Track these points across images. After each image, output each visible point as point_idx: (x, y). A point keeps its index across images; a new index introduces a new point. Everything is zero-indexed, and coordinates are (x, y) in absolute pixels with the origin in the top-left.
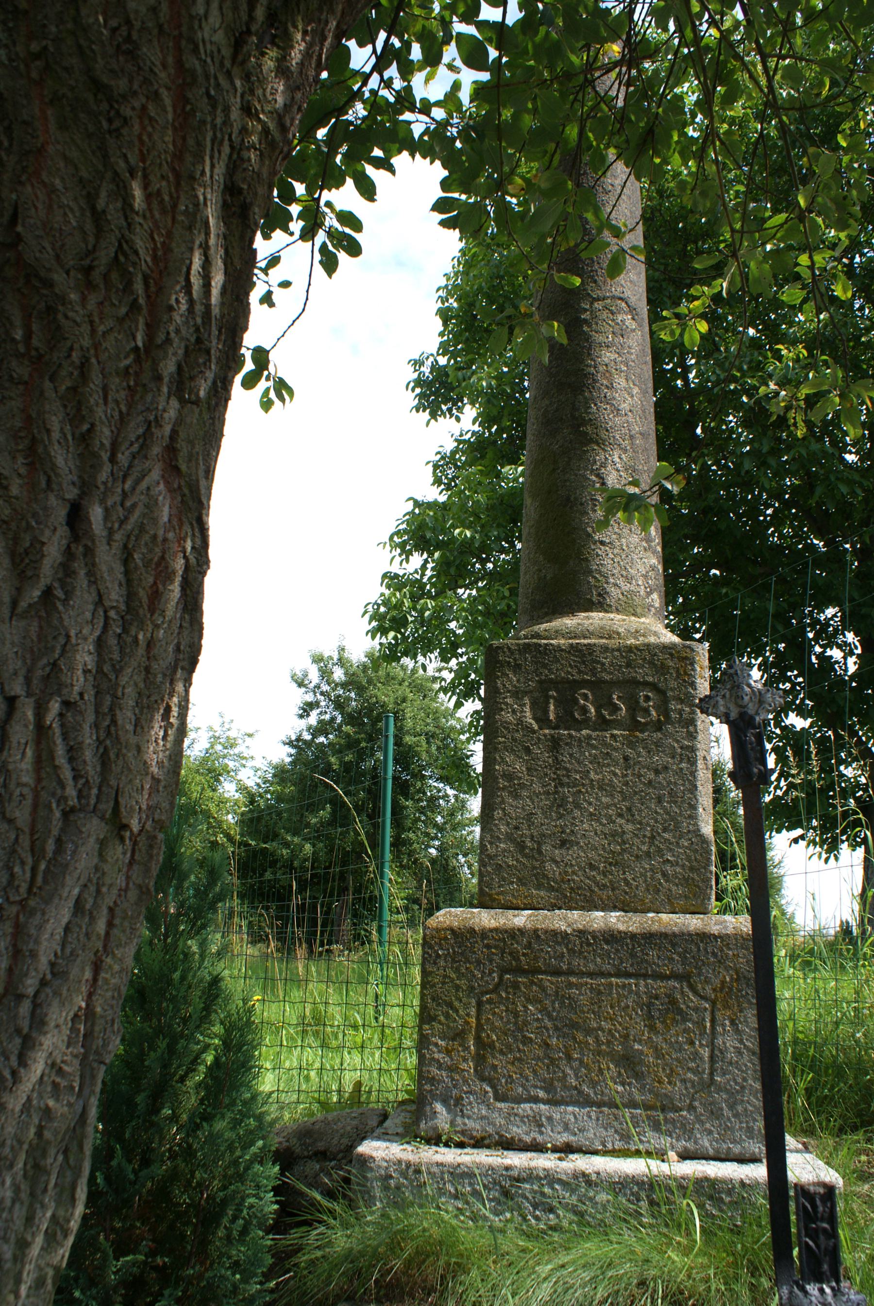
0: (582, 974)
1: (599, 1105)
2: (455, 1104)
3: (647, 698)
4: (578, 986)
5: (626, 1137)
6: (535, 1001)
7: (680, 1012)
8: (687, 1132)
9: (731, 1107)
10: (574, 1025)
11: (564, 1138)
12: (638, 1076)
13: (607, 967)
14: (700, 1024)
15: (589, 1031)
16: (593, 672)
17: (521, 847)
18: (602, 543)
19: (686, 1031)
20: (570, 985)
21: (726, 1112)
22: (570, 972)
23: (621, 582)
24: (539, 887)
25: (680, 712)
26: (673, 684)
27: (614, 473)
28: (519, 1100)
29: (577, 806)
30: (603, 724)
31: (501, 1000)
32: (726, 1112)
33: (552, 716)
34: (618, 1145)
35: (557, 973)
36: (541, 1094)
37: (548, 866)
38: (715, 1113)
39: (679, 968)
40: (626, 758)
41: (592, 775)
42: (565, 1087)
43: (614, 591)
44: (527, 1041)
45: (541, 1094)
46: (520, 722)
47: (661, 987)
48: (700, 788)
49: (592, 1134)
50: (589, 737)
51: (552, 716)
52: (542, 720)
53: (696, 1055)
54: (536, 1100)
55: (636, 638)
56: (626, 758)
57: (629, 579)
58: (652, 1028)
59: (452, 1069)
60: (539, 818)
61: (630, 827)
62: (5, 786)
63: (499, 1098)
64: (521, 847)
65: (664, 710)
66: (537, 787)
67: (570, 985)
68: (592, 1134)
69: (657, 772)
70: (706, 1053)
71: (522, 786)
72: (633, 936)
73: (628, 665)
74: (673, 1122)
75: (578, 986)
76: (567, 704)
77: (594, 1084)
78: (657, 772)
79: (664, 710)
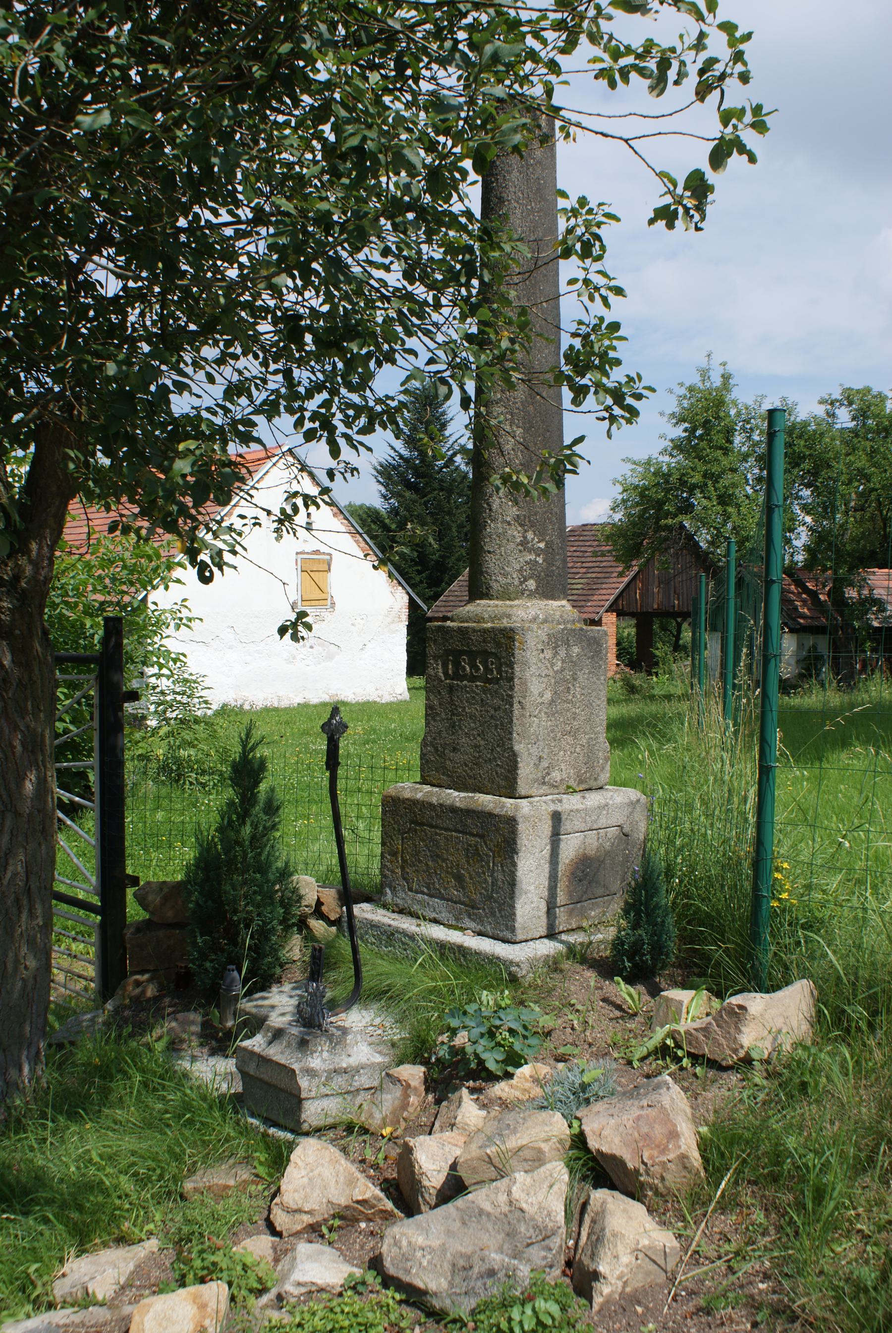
0: (441, 829)
1: (448, 900)
2: (394, 890)
3: (492, 663)
4: (440, 835)
5: (457, 919)
6: (423, 840)
7: (479, 855)
8: (482, 922)
9: (500, 912)
10: (438, 856)
11: (433, 915)
12: (463, 888)
13: (451, 826)
14: (488, 863)
15: (444, 860)
16: (468, 645)
17: (436, 750)
18: (489, 552)
19: (482, 866)
20: (436, 834)
21: (498, 914)
22: (436, 827)
23: (500, 578)
24: (443, 774)
25: (507, 672)
26: (504, 654)
27: (498, 500)
28: (417, 892)
29: (460, 728)
30: (473, 679)
31: (411, 838)
32: (498, 914)
33: (450, 672)
34: (454, 923)
35: (432, 826)
36: (425, 890)
37: (448, 762)
38: (493, 914)
39: (480, 831)
40: (482, 700)
41: (467, 710)
42: (435, 889)
43: (495, 585)
44: (420, 861)
45: (425, 890)
46: (436, 675)
47: (473, 840)
48: (515, 721)
49: (444, 916)
50: (466, 686)
51: (450, 672)
52: (446, 673)
53: (486, 881)
54: (423, 893)
55: (493, 622)
56: (482, 700)
57: (505, 575)
58: (468, 863)
59: (393, 872)
60: (444, 734)
61: (482, 743)
62: (885, 520)
63: (410, 890)
64: (436, 750)
65: (499, 672)
66: (444, 716)
67: (436, 834)
68: (444, 916)
69: (496, 710)
70: (490, 880)
71: (437, 714)
72: (461, 810)
73: (484, 641)
74: (476, 914)
75: (440, 835)
76: (457, 665)
77: (445, 889)
78: (496, 710)
79: (499, 672)
